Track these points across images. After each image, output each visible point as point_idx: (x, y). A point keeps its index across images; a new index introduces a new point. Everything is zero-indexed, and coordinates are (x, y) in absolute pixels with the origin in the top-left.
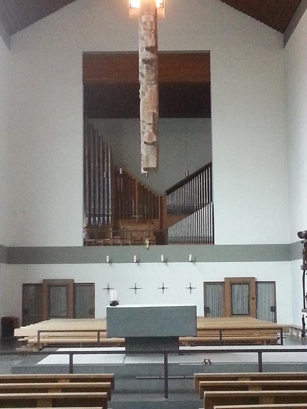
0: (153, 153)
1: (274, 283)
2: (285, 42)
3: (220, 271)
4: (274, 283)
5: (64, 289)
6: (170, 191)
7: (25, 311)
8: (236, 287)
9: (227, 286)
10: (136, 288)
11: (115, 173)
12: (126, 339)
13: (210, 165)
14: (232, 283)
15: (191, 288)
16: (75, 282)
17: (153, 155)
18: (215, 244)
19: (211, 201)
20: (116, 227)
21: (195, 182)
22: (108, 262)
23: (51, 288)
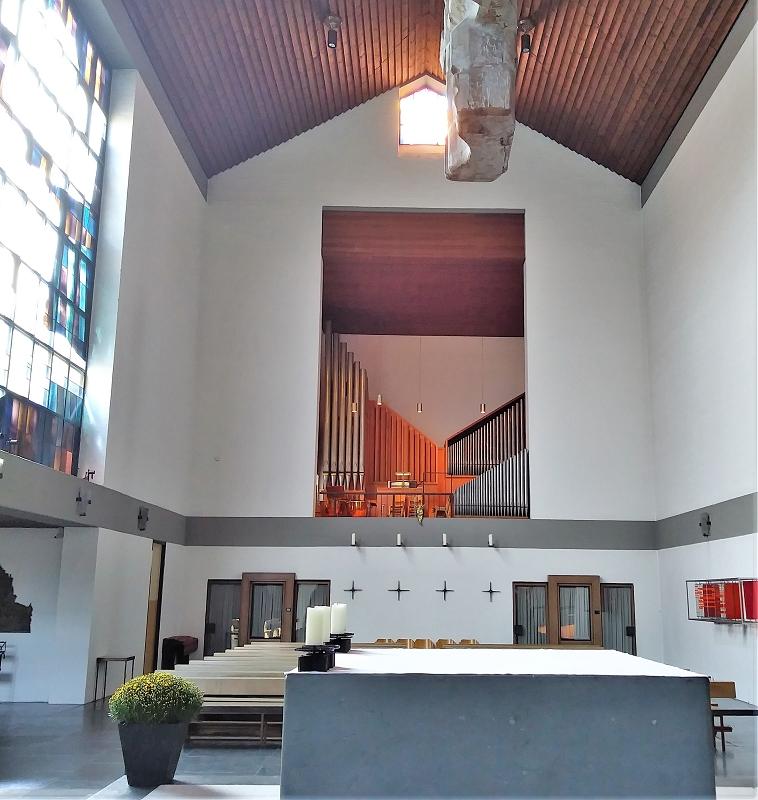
0: (498, 60)
1: (630, 586)
2: (644, 201)
3: (540, 564)
4: (630, 586)
5: (581, 593)
6: (452, 442)
7: (210, 628)
8: (565, 592)
9: (246, 586)
10: (399, 590)
11: (370, 405)
12: (332, 664)
13: (523, 397)
14: (561, 584)
15: (491, 592)
16: (299, 578)
17: (495, 65)
18: (532, 517)
19: (525, 447)
20: (131, 707)
21: (511, 412)
22: (353, 543)
23: (160, 546)
